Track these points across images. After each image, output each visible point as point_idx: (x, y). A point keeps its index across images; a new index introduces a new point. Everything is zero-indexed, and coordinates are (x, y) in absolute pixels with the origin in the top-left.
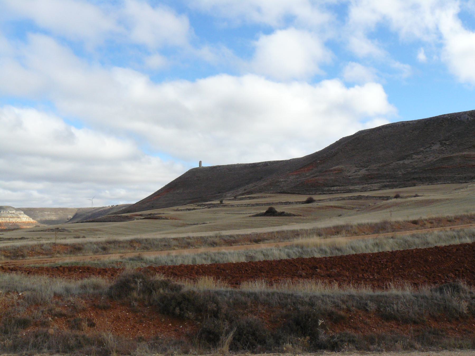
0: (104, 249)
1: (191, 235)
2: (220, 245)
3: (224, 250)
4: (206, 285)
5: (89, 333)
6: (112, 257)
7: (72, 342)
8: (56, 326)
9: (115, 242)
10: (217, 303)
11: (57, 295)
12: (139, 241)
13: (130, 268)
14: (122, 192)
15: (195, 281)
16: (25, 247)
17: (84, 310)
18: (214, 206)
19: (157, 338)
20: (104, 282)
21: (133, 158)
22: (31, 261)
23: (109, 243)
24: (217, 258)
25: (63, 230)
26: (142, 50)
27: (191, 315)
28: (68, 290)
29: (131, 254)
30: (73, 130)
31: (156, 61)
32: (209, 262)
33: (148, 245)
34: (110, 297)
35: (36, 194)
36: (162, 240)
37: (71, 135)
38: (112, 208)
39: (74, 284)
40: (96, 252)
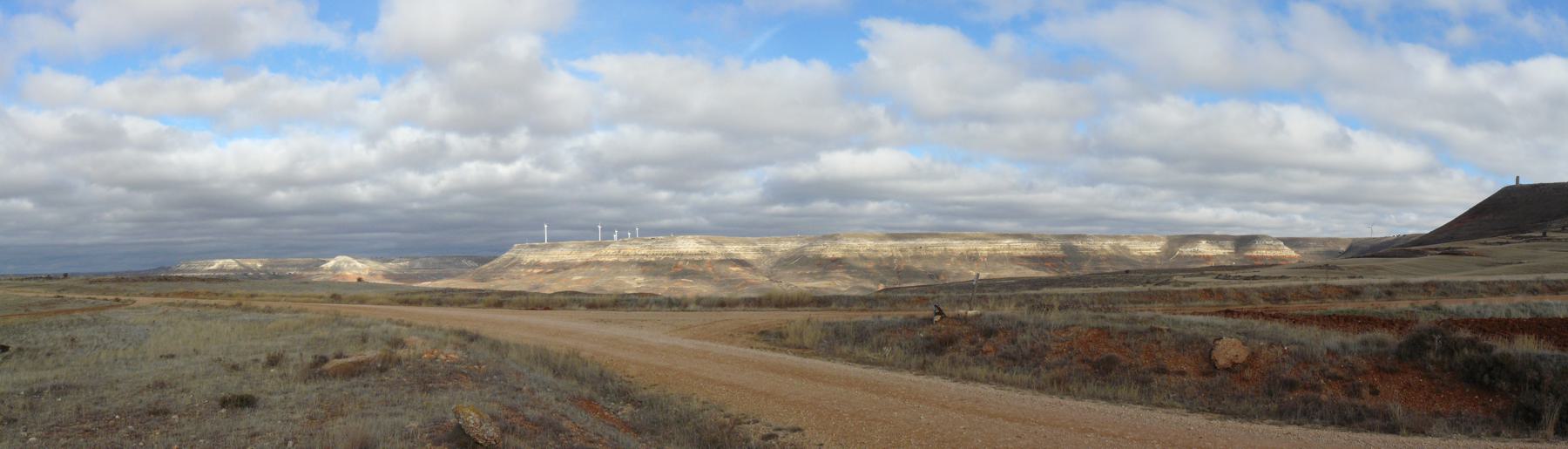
0: (1389, 293)
1: (1504, 278)
2: (1543, 293)
3: (1549, 299)
4: (1525, 346)
5: (1370, 402)
6: (1401, 305)
7: (1350, 413)
8: (1330, 392)
9: (1403, 285)
10: (1538, 370)
11: (1331, 352)
12: (1435, 285)
13: (1425, 320)
14: (1413, 218)
15: (1511, 340)
16: (1288, 288)
17: (1365, 373)
18: (1535, 239)
19: (1459, 414)
20: (1390, 337)
21: (1429, 171)
22: (1295, 307)
23: (1396, 285)
24: (1539, 311)
25: (1334, 267)
26: (1443, 19)
27: (1504, 385)
28: (1344, 346)
29: (1425, 302)
30: (1350, 132)
31: (1460, 35)
32: (1528, 316)
33: (1448, 290)
34: (1399, 356)
35: (1300, 219)
36: (1465, 284)
37: (1347, 139)
38: (1398, 238)
39: (1353, 339)
40: (1378, 298)
